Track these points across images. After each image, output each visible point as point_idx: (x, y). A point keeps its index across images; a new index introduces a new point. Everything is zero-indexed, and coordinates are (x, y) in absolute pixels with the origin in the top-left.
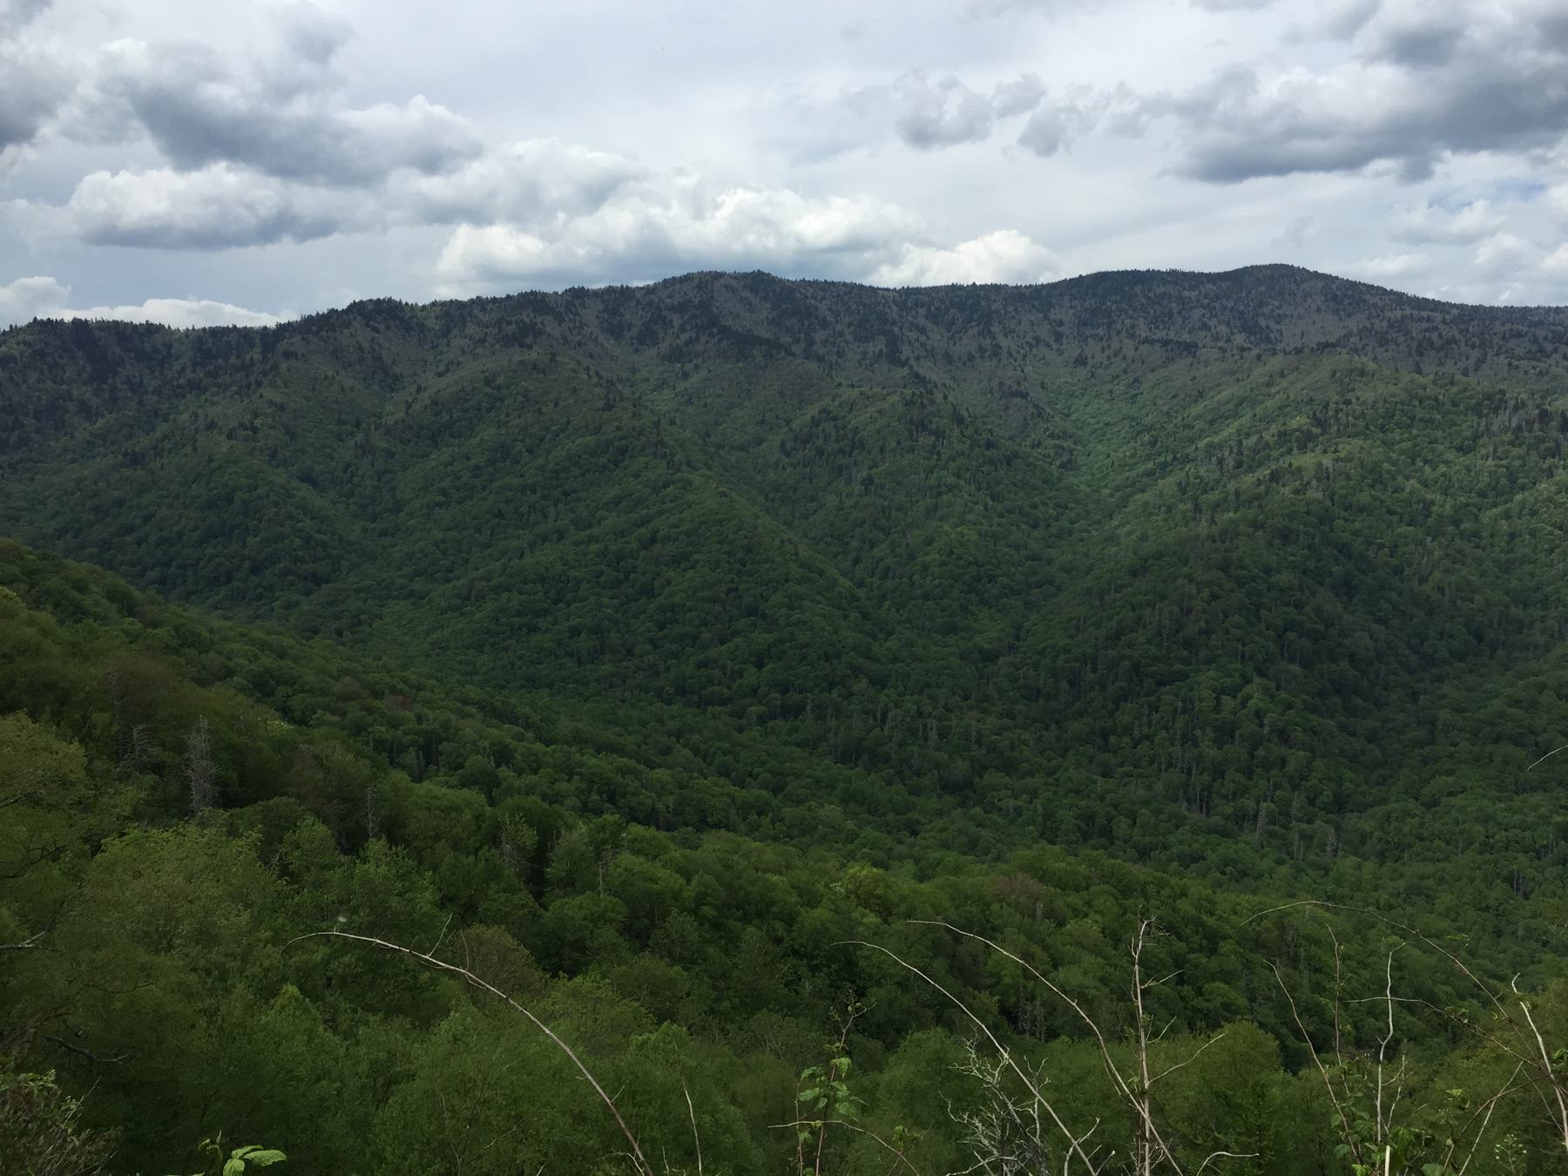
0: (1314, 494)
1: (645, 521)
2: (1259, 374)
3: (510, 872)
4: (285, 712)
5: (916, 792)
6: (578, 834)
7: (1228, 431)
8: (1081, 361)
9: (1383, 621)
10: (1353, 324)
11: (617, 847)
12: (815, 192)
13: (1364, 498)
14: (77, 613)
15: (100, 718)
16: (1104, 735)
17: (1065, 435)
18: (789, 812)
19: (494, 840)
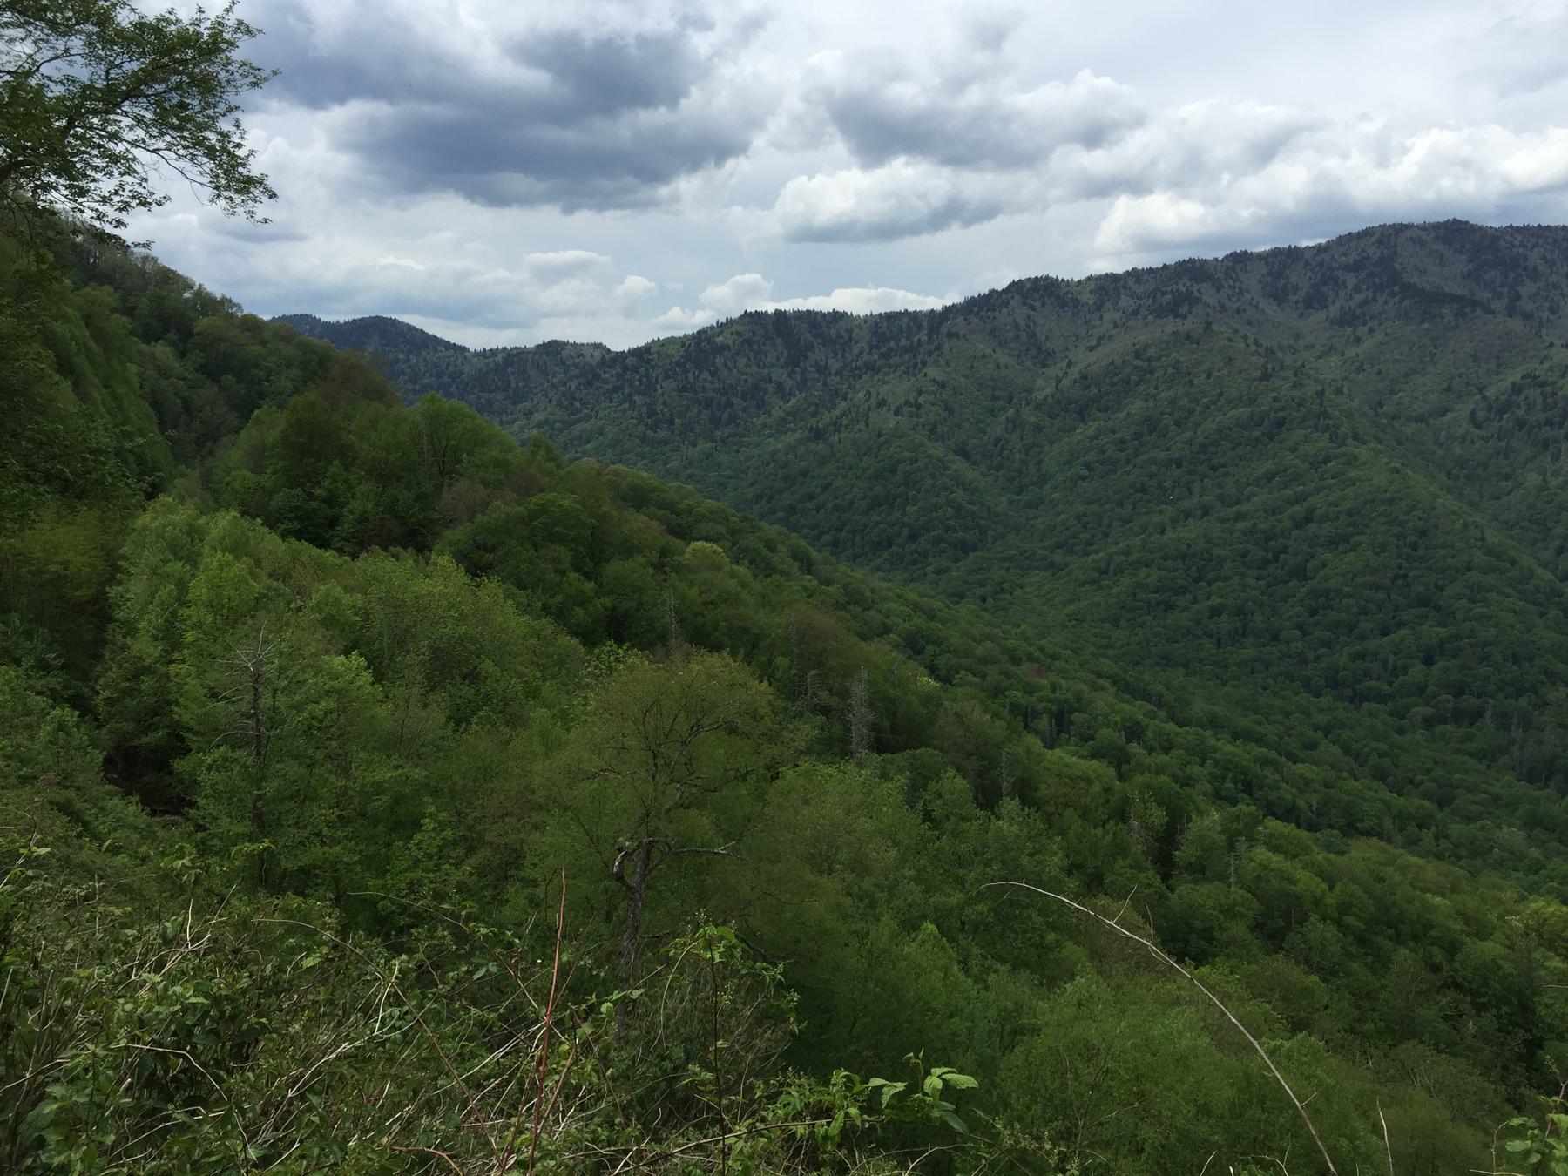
1: (1299, 499)
3: (1137, 849)
4: (932, 670)
6: (1209, 821)
11: (1252, 839)
12: (1528, 124)
18: (1457, 829)
19: (1122, 815)
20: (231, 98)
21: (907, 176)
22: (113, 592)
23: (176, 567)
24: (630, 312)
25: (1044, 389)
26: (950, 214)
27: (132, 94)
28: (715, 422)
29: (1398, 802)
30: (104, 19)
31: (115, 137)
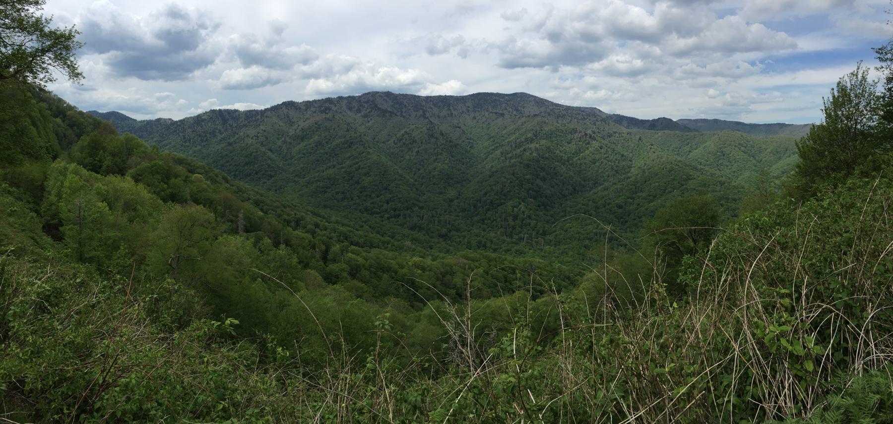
0: (535, 154)
1: (357, 163)
2: (520, 122)
3: (318, 256)
4: (262, 210)
5: (432, 237)
6: (336, 248)
7: (513, 138)
8: (474, 118)
9: (553, 187)
10: (542, 109)
11: (347, 252)
12: (404, 68)
13: (547, 155)
14: (216, 182)
15: (219, 207)
16: (483, 220)
17: (471, 139)
18: (396, 243)
19: (314, 247)
20: (74, 52)
21: (255, 70)
22: (45, 183)
23: (61, 178)
24: (180, 110)
25: (292, 132)
26: (268, 82)
27: (48, 51)
28: (202, 141)
29: (382, 238)
30: (42, 30)
31: (43, 63)
